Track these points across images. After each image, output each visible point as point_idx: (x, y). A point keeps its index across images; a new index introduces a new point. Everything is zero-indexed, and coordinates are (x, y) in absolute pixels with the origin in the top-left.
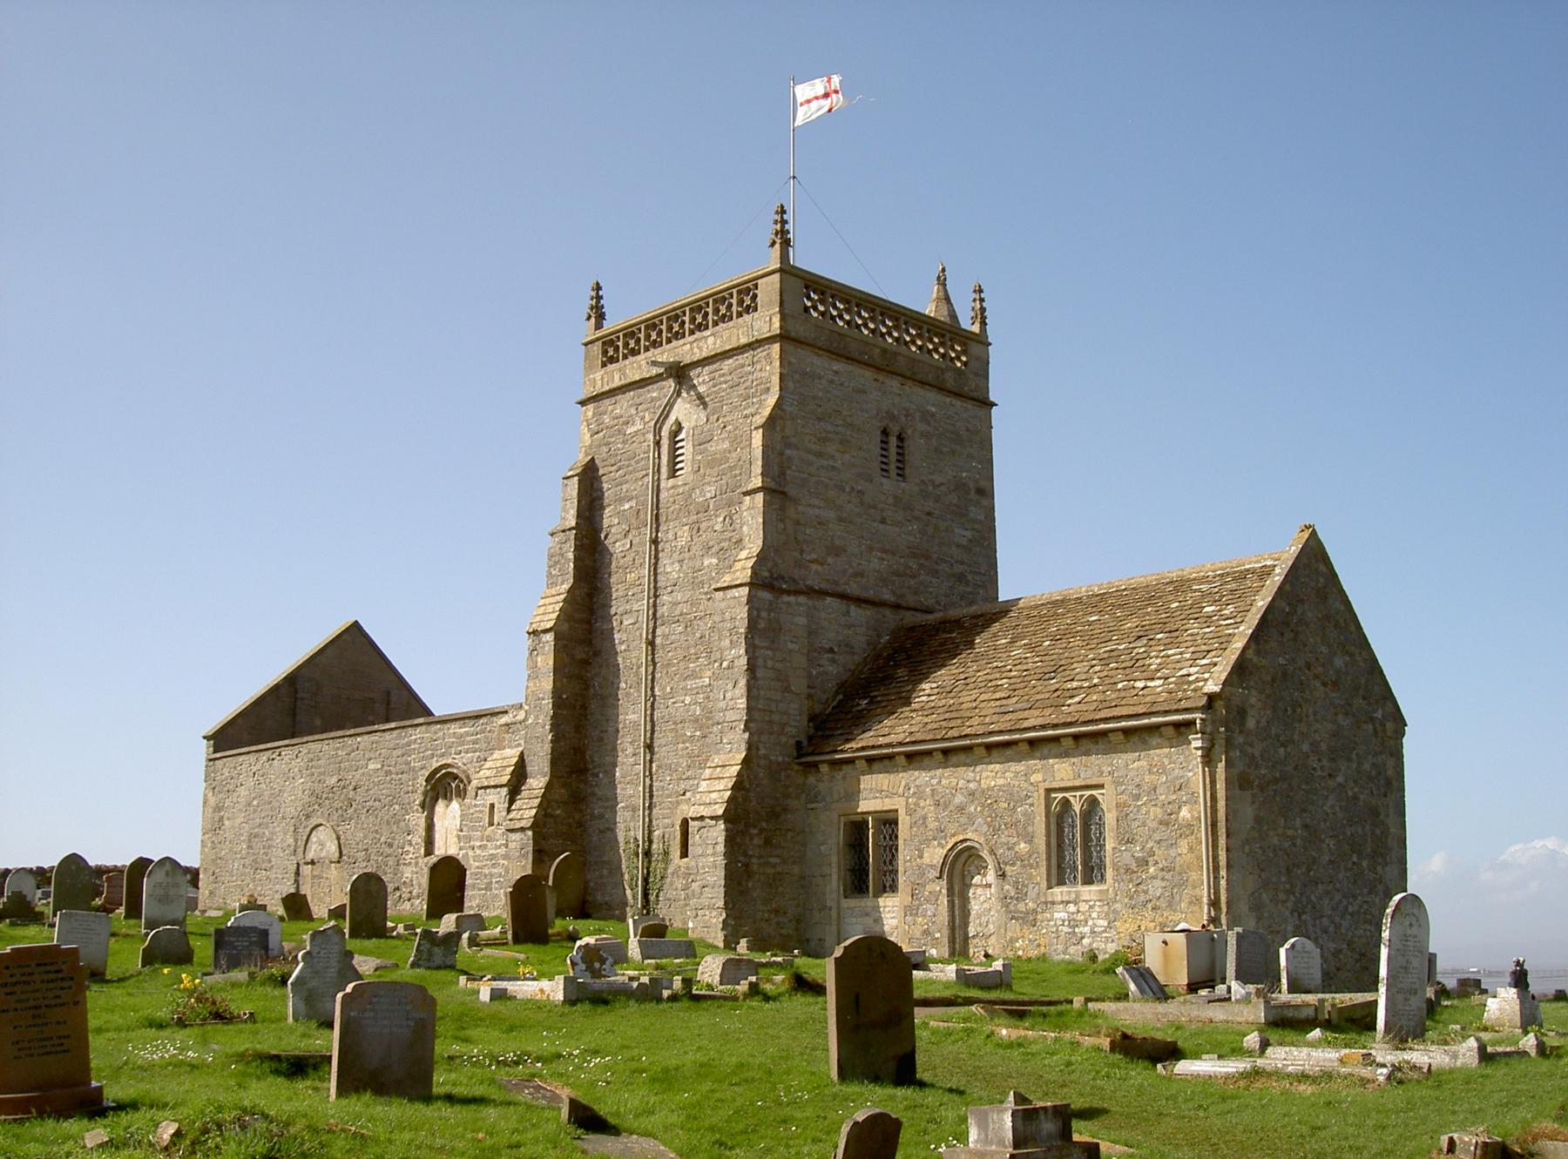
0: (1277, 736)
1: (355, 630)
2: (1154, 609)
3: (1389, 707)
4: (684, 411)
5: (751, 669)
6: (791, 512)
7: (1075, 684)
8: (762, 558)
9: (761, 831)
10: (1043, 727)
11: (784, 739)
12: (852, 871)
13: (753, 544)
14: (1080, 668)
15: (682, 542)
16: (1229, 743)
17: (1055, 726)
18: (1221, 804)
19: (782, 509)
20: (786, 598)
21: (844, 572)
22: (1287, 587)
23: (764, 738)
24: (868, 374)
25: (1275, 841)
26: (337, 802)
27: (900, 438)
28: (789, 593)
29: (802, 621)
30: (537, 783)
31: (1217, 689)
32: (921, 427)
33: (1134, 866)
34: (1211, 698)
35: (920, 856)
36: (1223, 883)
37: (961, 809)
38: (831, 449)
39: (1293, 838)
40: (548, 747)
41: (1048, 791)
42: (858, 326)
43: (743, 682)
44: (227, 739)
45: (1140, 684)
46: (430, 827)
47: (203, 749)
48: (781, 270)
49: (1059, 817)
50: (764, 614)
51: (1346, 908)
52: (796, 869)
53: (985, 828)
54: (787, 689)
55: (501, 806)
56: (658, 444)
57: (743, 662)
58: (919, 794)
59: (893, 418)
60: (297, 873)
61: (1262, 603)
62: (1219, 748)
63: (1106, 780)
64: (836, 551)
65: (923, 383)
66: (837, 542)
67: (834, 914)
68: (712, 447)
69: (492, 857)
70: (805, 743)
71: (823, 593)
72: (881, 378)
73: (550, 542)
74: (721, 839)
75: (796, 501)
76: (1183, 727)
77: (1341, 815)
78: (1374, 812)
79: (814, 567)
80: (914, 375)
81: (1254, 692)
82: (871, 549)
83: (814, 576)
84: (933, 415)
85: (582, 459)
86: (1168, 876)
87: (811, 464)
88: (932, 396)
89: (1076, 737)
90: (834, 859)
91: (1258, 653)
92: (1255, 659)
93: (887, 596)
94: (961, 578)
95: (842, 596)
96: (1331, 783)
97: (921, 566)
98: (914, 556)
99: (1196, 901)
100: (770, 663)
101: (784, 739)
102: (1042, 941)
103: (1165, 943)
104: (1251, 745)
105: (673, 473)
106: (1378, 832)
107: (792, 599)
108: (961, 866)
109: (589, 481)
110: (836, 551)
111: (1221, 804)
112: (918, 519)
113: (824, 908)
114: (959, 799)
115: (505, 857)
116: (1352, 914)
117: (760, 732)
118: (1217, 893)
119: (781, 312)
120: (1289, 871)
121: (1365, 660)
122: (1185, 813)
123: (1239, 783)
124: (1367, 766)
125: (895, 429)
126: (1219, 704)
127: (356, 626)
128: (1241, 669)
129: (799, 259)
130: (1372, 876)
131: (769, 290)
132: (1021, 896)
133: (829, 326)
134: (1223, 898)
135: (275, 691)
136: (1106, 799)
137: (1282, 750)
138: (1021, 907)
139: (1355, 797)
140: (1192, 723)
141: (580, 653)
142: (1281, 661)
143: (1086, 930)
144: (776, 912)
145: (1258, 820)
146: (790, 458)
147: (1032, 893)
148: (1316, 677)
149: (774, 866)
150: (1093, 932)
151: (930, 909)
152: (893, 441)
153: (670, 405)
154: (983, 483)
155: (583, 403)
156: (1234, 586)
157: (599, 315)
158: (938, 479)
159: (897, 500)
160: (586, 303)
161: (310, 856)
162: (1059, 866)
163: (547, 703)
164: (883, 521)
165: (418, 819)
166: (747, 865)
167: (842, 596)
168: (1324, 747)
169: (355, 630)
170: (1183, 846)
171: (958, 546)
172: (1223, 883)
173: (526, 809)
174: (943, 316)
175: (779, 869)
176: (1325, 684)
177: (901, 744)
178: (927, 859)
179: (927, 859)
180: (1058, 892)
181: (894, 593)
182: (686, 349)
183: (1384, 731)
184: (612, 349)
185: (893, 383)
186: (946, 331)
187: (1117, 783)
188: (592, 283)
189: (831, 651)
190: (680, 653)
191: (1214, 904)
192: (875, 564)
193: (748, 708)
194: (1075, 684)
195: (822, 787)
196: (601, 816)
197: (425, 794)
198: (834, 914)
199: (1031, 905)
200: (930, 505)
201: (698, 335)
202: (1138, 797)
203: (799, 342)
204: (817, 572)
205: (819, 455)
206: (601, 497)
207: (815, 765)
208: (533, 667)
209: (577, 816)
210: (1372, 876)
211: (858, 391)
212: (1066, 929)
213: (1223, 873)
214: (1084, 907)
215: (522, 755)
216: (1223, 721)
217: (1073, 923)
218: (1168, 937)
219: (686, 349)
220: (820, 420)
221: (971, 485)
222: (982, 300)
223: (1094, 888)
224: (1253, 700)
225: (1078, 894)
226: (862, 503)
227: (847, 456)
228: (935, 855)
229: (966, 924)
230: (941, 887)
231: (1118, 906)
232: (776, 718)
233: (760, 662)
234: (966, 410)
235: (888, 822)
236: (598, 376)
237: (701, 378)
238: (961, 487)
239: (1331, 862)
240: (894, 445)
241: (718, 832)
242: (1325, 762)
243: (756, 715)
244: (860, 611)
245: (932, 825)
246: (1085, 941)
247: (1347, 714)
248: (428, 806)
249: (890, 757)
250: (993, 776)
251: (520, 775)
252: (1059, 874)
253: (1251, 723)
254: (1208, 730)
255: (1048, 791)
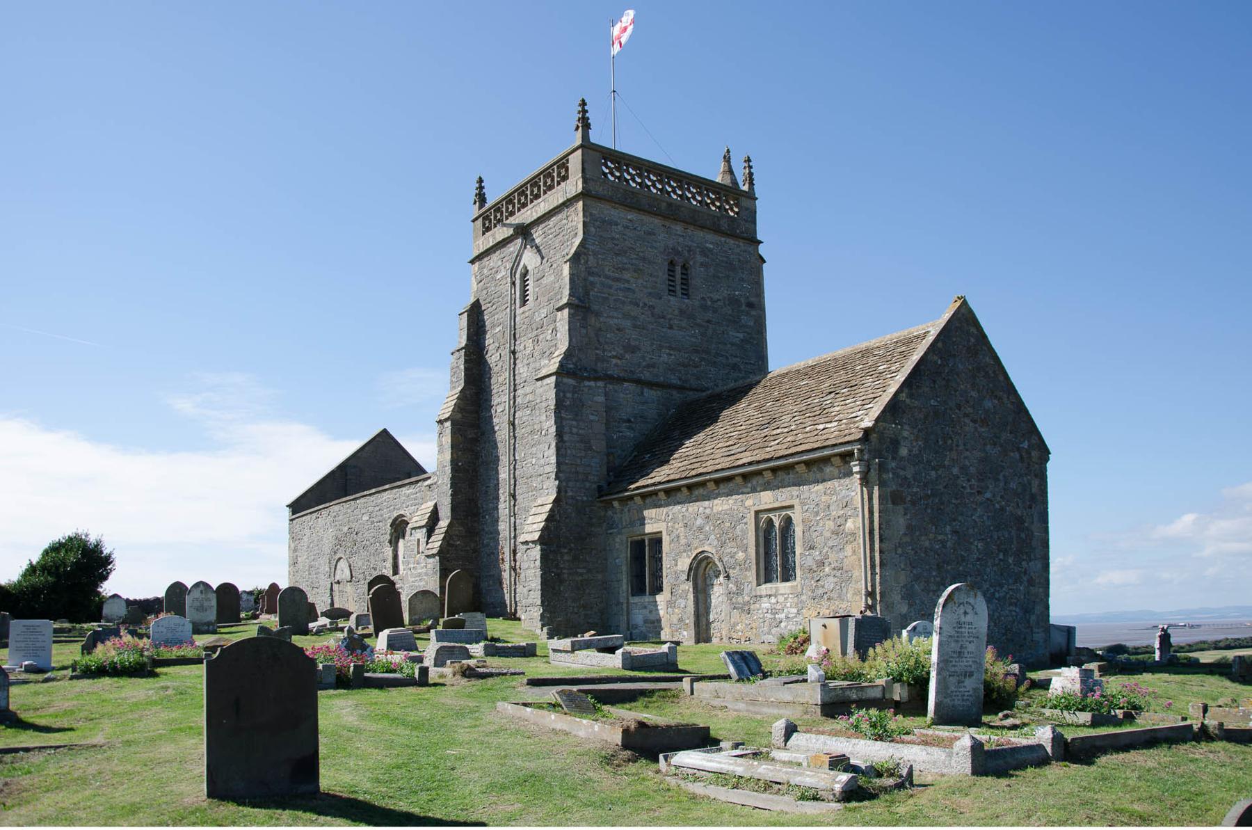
0: (929, 462)
1: (385, 433)
2: (841, 374)
3: (1034, 440)
4: (530, 259)
5: (559, 435)
6: (592, 320)
7: (778, 431)
8: (568, 355)
9: (571, 550)
10: (750, 464)
11: (588, 485)
12: (637, 576)
13: (563, 346)
14: (787, 418)
15: (528, 351)
16: (882, 468)
17: (758, 462)
18: (876, 515)
19: (584, 318)
20: (587, 383)
21: (639, 365)
22: (940, 345)
23: (571, 484)
24: (657, 221)
25: (927, 544)
26: (347, 542)
27: (684, 267)
28: (589, 379)
29: (601, 399)
30: (443, 524)
31: (870, 424)
32: (699, 258)
33: (814, 567)
34: (867, 432)
35: (675, 565)
36: (878, 577)
37: (700, 529)
38: (627, 276)
39: (943, 543)
40: (449, 499)
41: (757, 513)
42: (708, 205)
43: (554, 444)
44: (299, 506)
45: (821, 427)
46: (395, 557)
47: (287, 513)
48: (581, 146)
49: (765, 534)
50: (569, 395)
51: (993, 594)
52: (600, 577)
53: (715, 543)
54: (590, 448)
55: (423, 540)
56: (514, 283)
57: (553, 429)
58: (674, 520)
59: (678, 253)
60: (332, 590)
61: (915, 358)
62: (873, 474)
63: (795, 502)
64: (633, 350)
65: (702, 227)
66: (633, 343)
67: (625, 606)
68: (544, 281)
69: (420, 574)
70: (605, 486)
71: (620, 380)
72: (667, 224)
73: (453, 359)
74: (538, 557)
75: (597, 314)
76: (847, 457)
77: (988, 523)
78: (1020, 520)
79: (614, 361)
80: (694, 219)
81: (906, 427)
82: (661, 346)
83: (614, 367)
84: (710, 250)
85: (472, 300)
86: (838, 574)
87: (610, 287)
88: (710, 237)
89: (774, 470)
90: (624, 568)
91: (911, 396)
92: (908, 401)
93: (675, 381)
94: (735, 367)
95: (638, 382)
96: (979, 498)
97: (702, 359)
98: (697, 351)
99: (857, 593)
100: (575, 430)
101: (588, 485)
102: (754, 625)
103: (825, 626)
104: (904, 469)
105: (524, 302)
106: (1023, 536)
107: (592, 383)
108: (702, 573)
109: (476, 315)
110: (633, 350)
111: (876, 515)
112: (699, 325)
113: (619, 603)
114: (699, 522)
115: (426, 574)
116: (998, 599)
117: (568, 480)
118: (873, 586)
119: (583, 177)
120: (939, 567)
121: (1013, 403)
122: (850, 525)
123: (892, 500)
124: (1013, 485)
125: (679, 261)
126: (874, 437)
127: (385, 432)
128: (893, 408)
129: (595, 138)
130: (1016, 569)
131: (575, 162)
132: (739, 593)
133: (621, 189)
134: (878, 591)
135: (331, 475)
136: (797, 516)
137: (933, 473)
138: (740, 599)
139: (1002, 509)
140: (851, 454)
141: (471, 434)
142: (932, 402)
143: (783, 616)
144: (584, 607)
145: (910, 528)
146: (592, 283)
147: (747, 590)
148: (966, 415)
149: (581, 574)
150: (787, 618)
151: (682, 602)
152: (678, 269)
153: (519, 256)
154: (753, 299)
155: (472, 262)
156: (903, 349)
157: (481, 198)
158: (716, 297)
159: (682, 312)
160: (474, 191)
161: (337, 578)
162: (766, 569)
163: (448, 469)
164: (671, 327)
165: (388, 551)
166: (558, 575)
167: (638, 382)
168: (973, 470)
169: (385, 433)
170: (849, 549)
171: (733, 344)
172: (878, 577)
173: (437, 542)
174: (727, 181)
175: (585, 577)
176: (974, 421)
177: (660, 483)
178: (680, 567)
179: (680, 567)
180: (766, 588)
181: (680, 379)
182: (526, 215)
183: (1030, 457)
184: (488, 220)
185: (678, 228)
186: (729, 192)
187: (803, 504)
188: (477, 179)
189: (629, 421)
190: (529, 429)
191: (871, 594)
192: (665, 358)
193: (557, 463)
194: (778, 431)
195: (616, 517)
196: (488, 545)
197: (391, 535)
198: (625, 606)
199: (747, 598)
200: (709, 315)
201: (535, 202)
202: (817, 514)
203: (599, 198)
204: (616, 365)
205: (618, 280)
206: (484, 326)
207: (610, 503)
208: (441, 445)
209: (473, 545)
210: (1016, 569)
211: (650, 234)
212: (769, 616)
213: (878, 570)
214: (781, 599)
215: (435, 506)
216: (877, 451)
217: (774, 611)
218: (827, 621)
219: (526, 215)
220: (617, 255)
221: (743, 300)
222: (750, 167)
223: (788, 584)
224: (905, 434)
225: (777, 590)
226: (653, 315)
227: (640, 281)
228: (685, 563)
229: (708, 613)
230: (689, 586)
231: (804, 597)
232: (580, 469)
233: (566, 429)
234: (738, 246)
235: (657, 541)
236: (480, 242)
237: (538, 234)
238: (734, 301)
239: (978, 559)
240: (679, 275)
241: (536, 552)
242: (973, 482)
243: (564, 467)
244: (653, 392)
245: (683, 541)
246: (783, 625)
247: (995, 444)
248: (394, 542)
249: (655, 493)
250: (721, 505)
251: (434, 517)
252: (767, 575)
253: (904, 452)
254: (866, 457)
255: (757, 513)
